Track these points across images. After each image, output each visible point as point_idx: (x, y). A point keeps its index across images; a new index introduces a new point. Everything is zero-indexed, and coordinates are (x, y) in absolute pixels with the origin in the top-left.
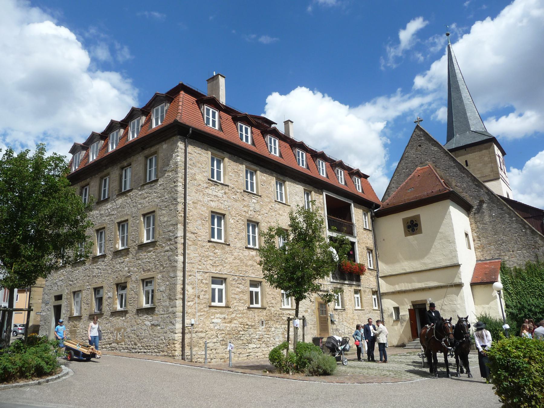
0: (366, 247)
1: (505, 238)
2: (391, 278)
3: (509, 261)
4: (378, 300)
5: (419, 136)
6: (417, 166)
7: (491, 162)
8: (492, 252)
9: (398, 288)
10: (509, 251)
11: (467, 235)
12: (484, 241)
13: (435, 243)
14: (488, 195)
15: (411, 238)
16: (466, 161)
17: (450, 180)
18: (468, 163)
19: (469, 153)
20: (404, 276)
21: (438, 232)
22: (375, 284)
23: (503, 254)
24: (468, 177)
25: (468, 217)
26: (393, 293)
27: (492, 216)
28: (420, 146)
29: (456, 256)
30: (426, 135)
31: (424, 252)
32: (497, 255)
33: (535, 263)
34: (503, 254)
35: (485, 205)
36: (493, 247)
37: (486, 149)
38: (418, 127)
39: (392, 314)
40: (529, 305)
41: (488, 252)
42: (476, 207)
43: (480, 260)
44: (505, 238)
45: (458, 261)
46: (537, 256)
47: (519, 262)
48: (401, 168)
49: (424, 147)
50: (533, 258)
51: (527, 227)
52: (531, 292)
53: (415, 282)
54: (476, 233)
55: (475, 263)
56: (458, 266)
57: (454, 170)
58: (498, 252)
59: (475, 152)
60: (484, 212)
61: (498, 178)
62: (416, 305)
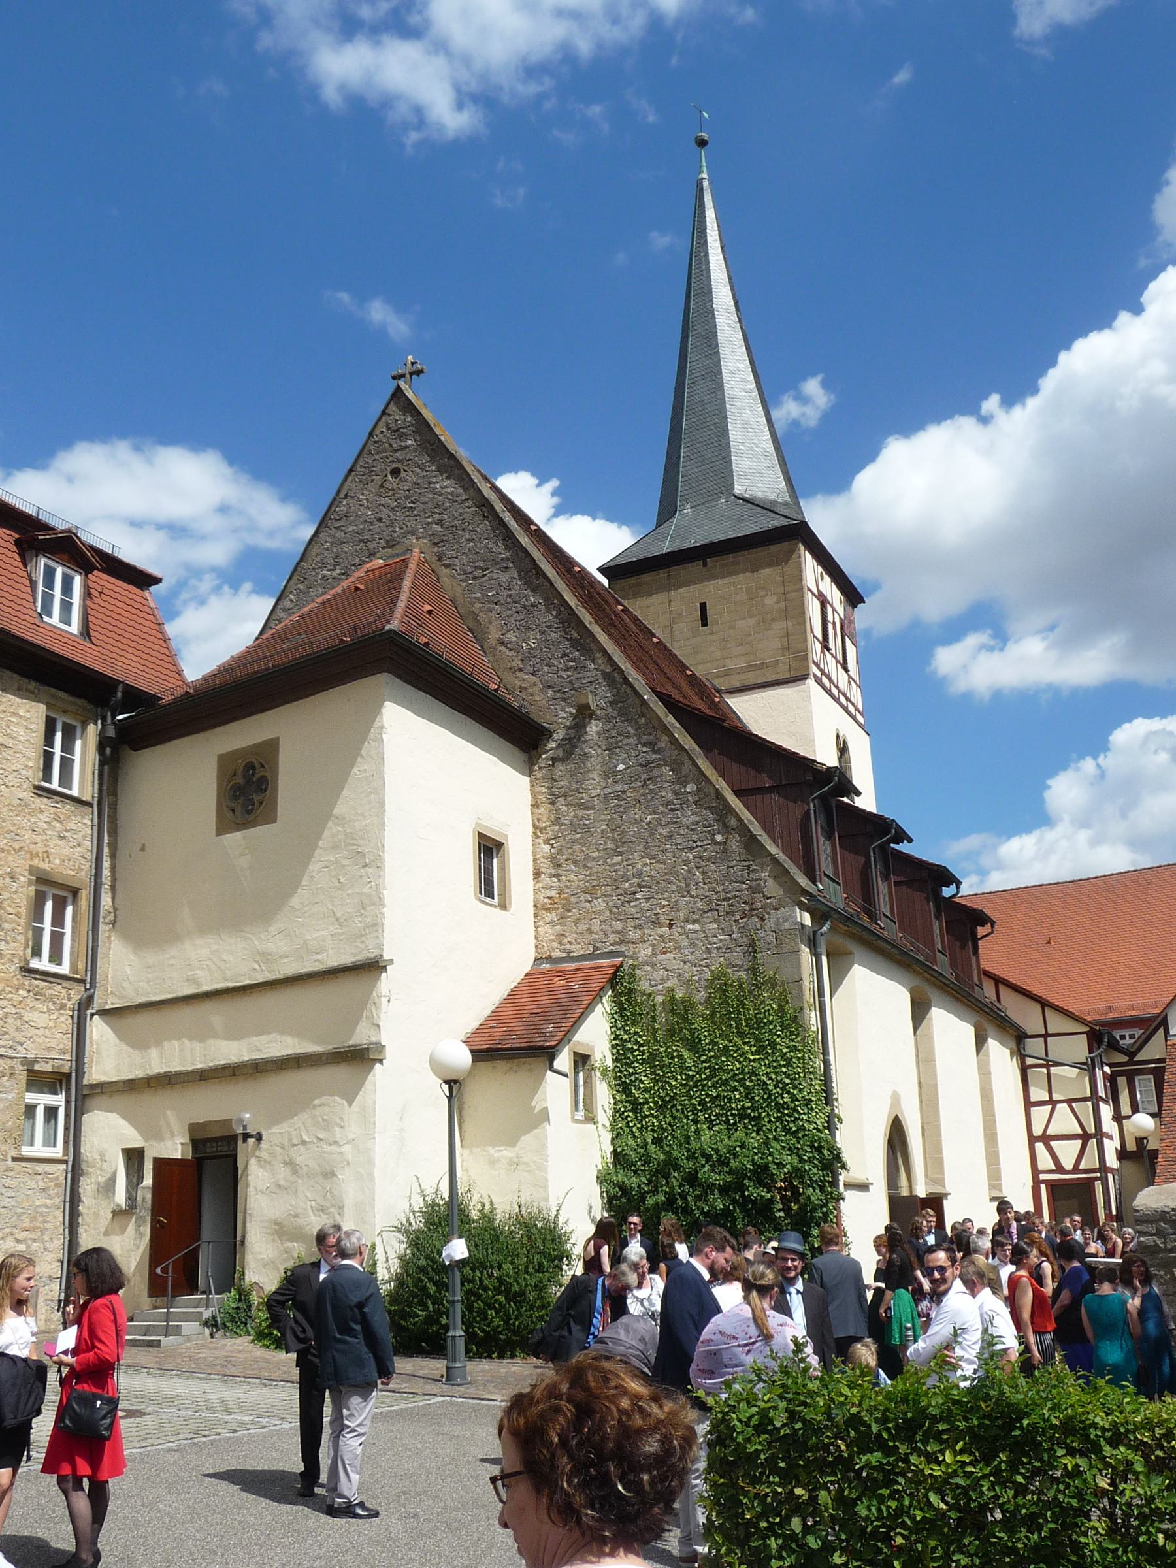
0: (32, 870)
1: (649, 869)
2: (142, 1019)
3: (653, 965)
4: (67, 1115)
5: (398, 433)
6: (372, 555)
7: (785, 614)
8: (596, 925)
9: (157, 1062)
10: (656, 923)
11: (489, 848)
12: (573, 877)
13: (313, 867)
14: (612, 683)
15: (235, 839)
16: (703, 607)
17: (483, 617)
18: (710, 613)
19: (714, 577)
20: (185, 1013)
21: (329, 815)
22: (67, 1042)
23: (633, 935)
24: (549, 605)
25: (528, 768)
26: (131, 1086)
27: (615, 773)
28: (396, 472)
29: (376, 926)
30: (422, 426)
31: (259, 904)
32: (613, 938)
33: (743, 975)
34: (633, 935)
35: (594, 728)
36: (600, 904)
37: (773, 563)
38: (398, 393)
39: (112, 1180)
40: (691, 1156)
41: (582, 927)
42: (560, 734)
43: (549, 959)
44: (649, 869)
45: (380, 946)
46: (752, 948)
47: (689, 971)
48: (314, 559)
49: (409, 476)
50: (737, 956)
51: (733, 822)
52: (714, 1099)
53: (216, 1037)
54: (547, 841)
55: (527, 968)
56: (373, 967)
57: (504, 577)
58: (618, 925)
59: (737, 573)
60: (586, 756)
61: (803, 678)
62: (206, 1141)
